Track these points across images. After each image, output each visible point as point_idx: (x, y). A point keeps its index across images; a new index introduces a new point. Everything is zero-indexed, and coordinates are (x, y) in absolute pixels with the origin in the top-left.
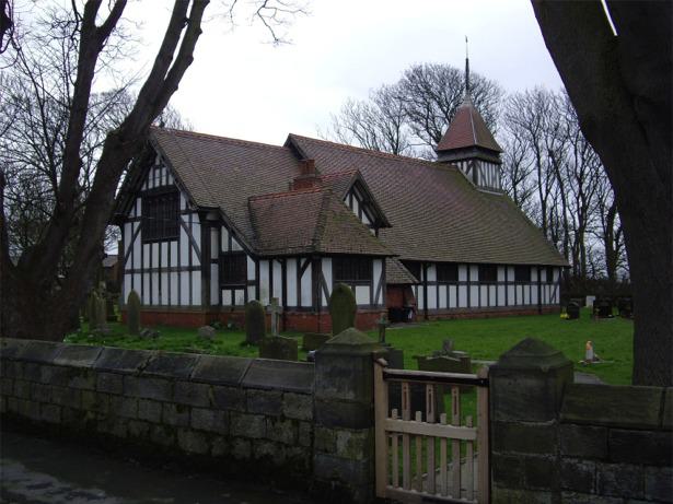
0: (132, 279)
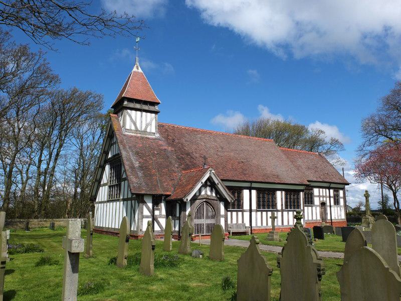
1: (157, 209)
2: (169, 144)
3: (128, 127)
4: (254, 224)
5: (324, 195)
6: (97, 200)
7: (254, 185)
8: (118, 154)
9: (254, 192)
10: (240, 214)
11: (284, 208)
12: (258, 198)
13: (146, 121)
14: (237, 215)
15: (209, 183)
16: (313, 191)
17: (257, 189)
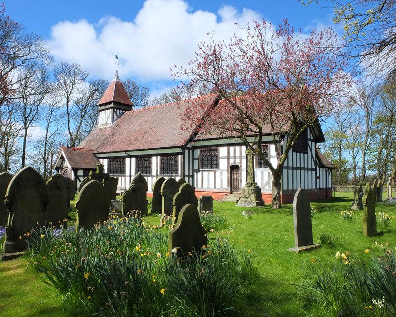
0: (288, 173)
9: (133, 159)
12: (137, 164)
14: (209, 175)
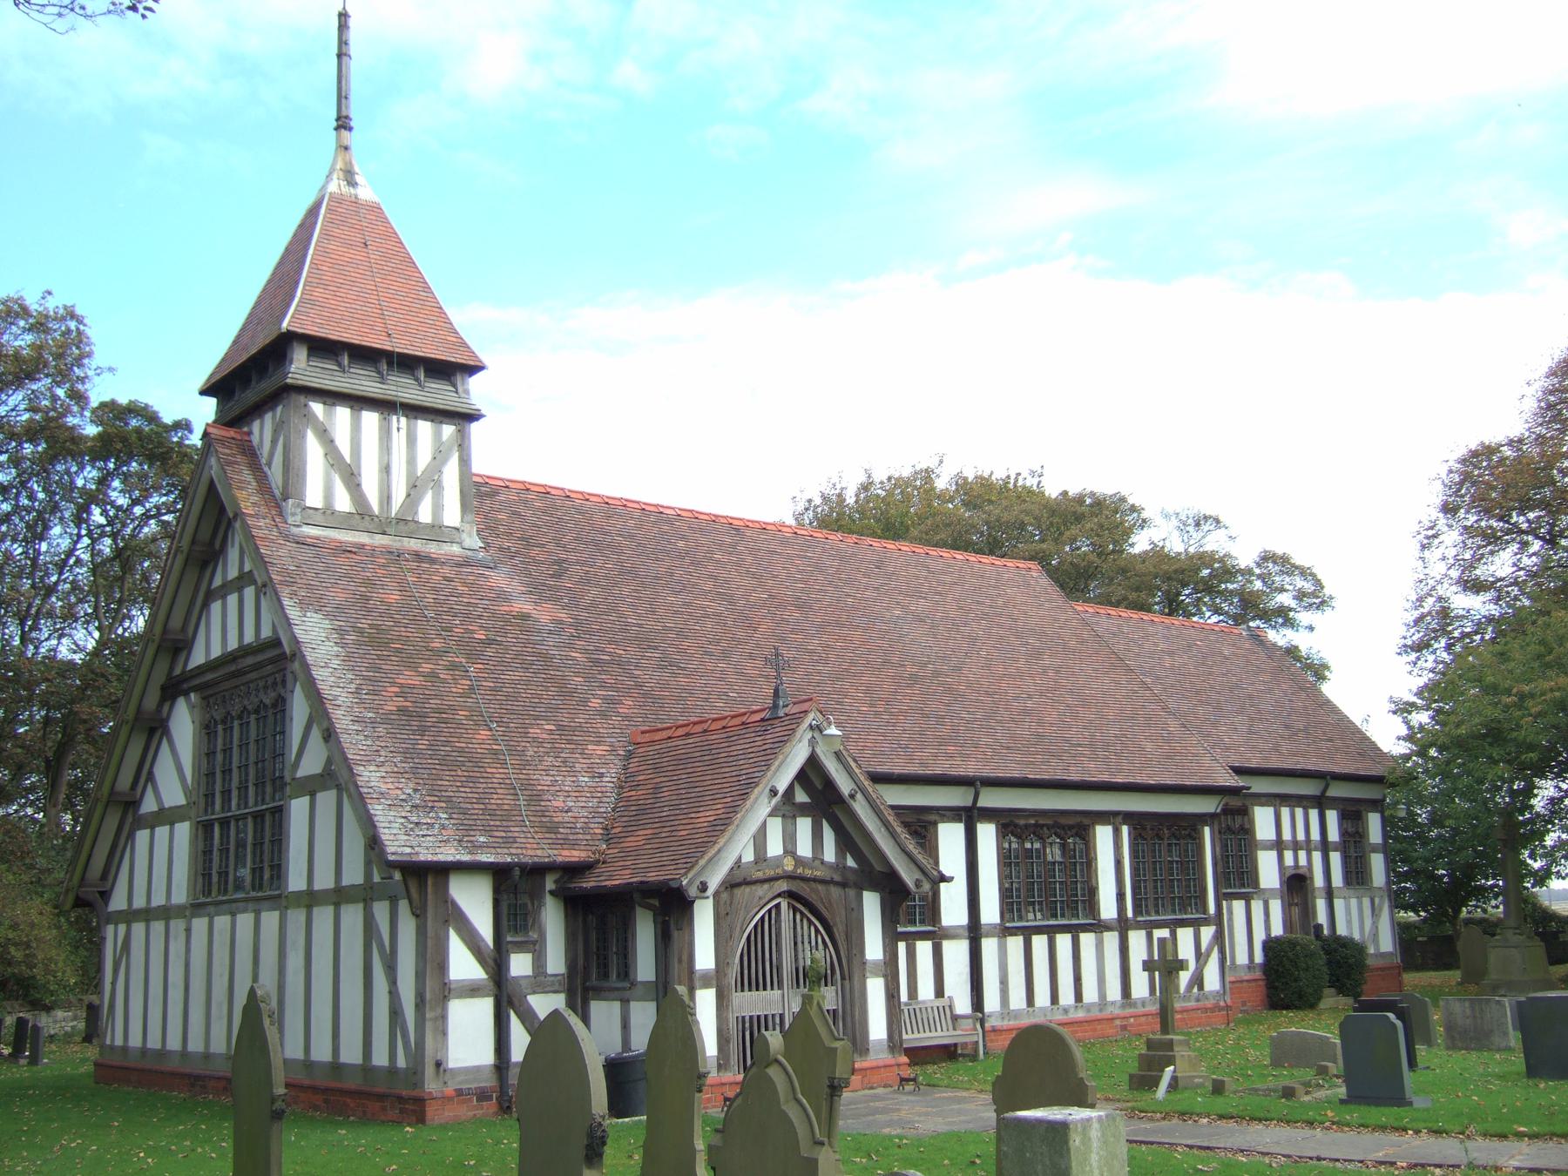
1: (521, 947)
2: (538, 591)
3: (314, 496)
4: (991, 1002)
5: (1301, 836)
6: (118, 902)
7: (991, 799)
8: (275, 643)
9: (987, 834)
10: (924, 949)
11: (1130, 914)
13: (411, 461)
15: (801, 797)
16: (1252, 822)
17: (1008, 823)
